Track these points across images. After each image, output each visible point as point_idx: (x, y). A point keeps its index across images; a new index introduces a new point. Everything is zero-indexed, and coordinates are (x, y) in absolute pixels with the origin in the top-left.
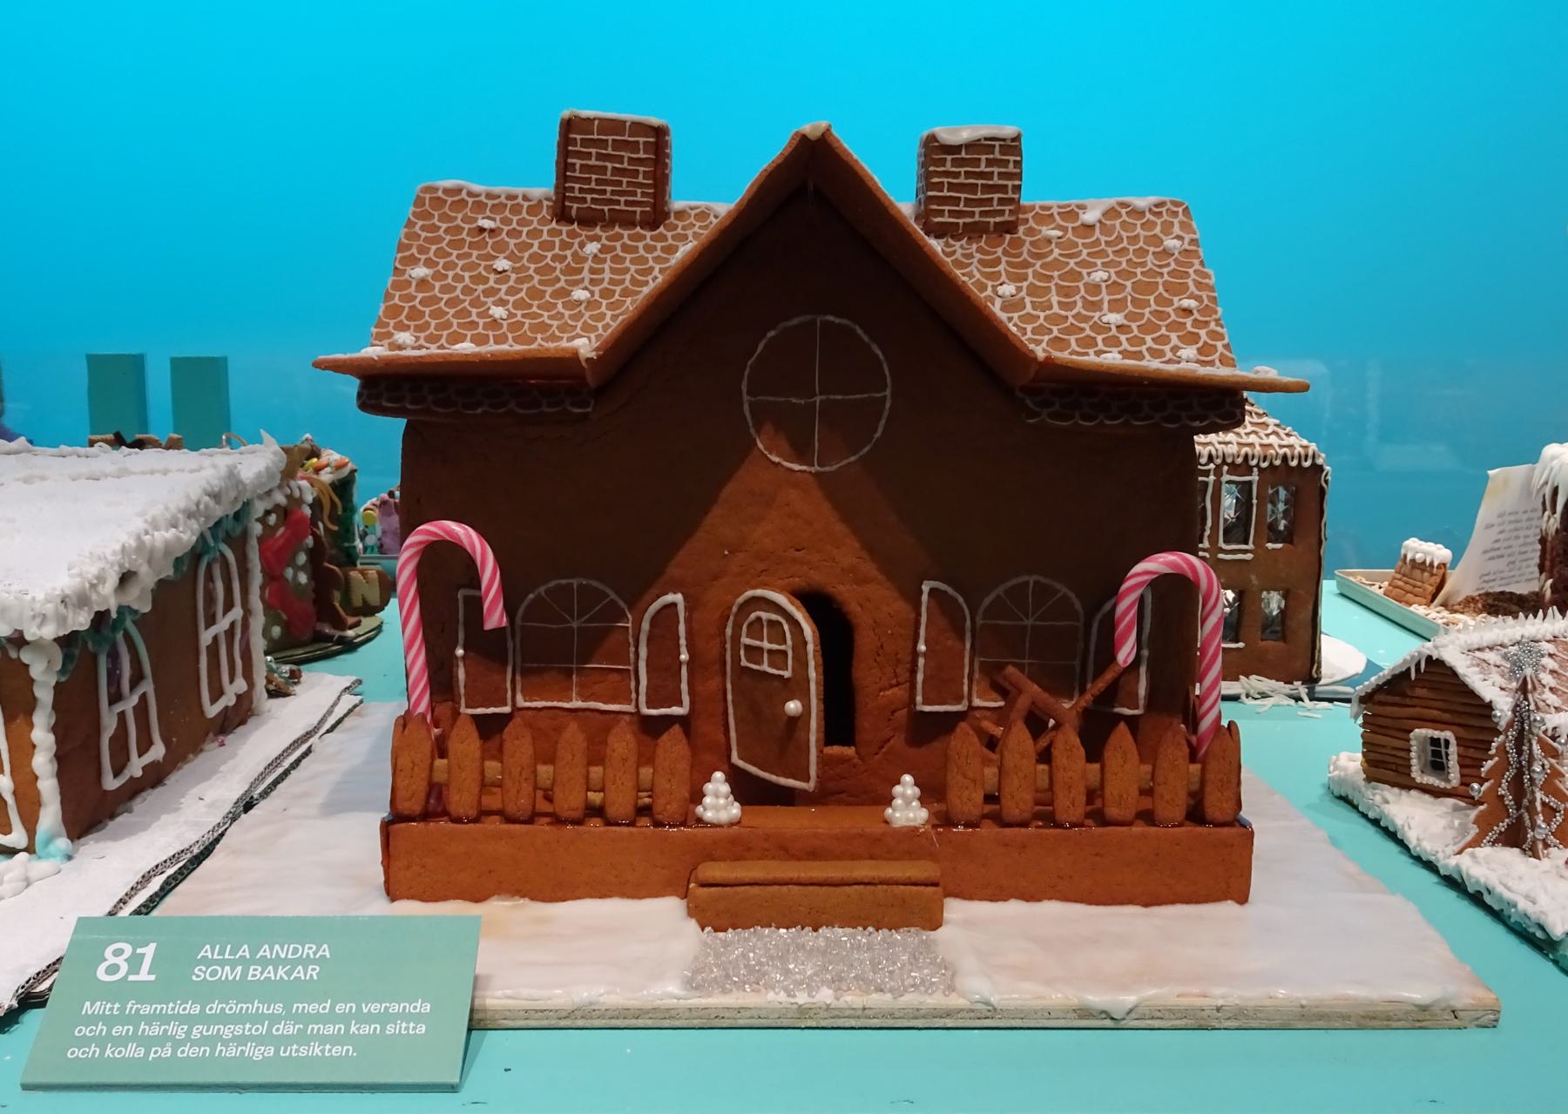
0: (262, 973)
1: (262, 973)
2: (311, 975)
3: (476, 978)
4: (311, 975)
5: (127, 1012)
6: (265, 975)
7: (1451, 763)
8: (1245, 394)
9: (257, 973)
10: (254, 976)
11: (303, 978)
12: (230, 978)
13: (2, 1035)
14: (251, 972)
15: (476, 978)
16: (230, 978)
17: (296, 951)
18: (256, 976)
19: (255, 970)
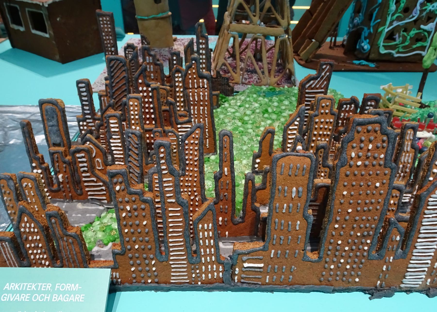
0: (58, 298)
1: (58, 298)
2: (12, 288)
3: (215, 204)
4: (12, 288)
5: (122, 156)
6: (59, 299)
7: (60, 117)
8: (253, 6)
9: (56, 298)
10: (55, 299)
11: (19, 300)
12: (74, 290)
13: (153, 2)
14: (54, 297)
15: (215, 204)
16: (74, 290)
17: (63, 287)
18: (30, 285)
19: (55, 296)
